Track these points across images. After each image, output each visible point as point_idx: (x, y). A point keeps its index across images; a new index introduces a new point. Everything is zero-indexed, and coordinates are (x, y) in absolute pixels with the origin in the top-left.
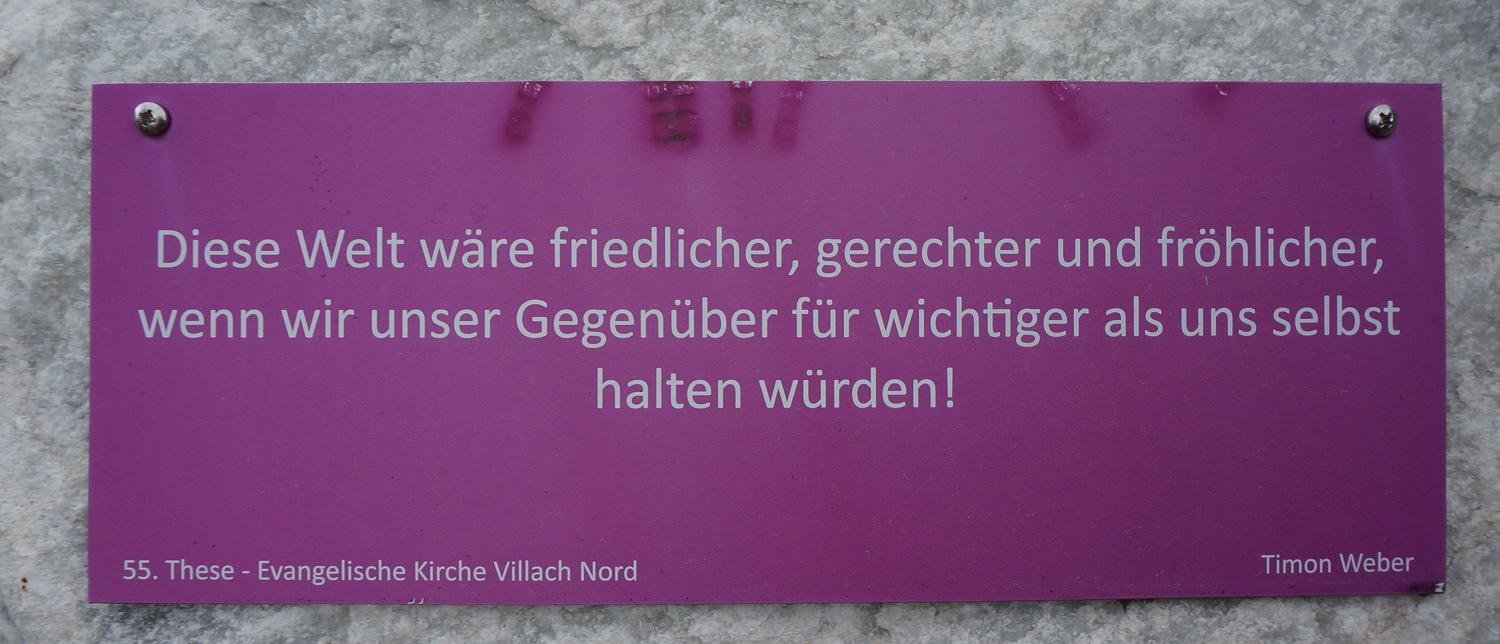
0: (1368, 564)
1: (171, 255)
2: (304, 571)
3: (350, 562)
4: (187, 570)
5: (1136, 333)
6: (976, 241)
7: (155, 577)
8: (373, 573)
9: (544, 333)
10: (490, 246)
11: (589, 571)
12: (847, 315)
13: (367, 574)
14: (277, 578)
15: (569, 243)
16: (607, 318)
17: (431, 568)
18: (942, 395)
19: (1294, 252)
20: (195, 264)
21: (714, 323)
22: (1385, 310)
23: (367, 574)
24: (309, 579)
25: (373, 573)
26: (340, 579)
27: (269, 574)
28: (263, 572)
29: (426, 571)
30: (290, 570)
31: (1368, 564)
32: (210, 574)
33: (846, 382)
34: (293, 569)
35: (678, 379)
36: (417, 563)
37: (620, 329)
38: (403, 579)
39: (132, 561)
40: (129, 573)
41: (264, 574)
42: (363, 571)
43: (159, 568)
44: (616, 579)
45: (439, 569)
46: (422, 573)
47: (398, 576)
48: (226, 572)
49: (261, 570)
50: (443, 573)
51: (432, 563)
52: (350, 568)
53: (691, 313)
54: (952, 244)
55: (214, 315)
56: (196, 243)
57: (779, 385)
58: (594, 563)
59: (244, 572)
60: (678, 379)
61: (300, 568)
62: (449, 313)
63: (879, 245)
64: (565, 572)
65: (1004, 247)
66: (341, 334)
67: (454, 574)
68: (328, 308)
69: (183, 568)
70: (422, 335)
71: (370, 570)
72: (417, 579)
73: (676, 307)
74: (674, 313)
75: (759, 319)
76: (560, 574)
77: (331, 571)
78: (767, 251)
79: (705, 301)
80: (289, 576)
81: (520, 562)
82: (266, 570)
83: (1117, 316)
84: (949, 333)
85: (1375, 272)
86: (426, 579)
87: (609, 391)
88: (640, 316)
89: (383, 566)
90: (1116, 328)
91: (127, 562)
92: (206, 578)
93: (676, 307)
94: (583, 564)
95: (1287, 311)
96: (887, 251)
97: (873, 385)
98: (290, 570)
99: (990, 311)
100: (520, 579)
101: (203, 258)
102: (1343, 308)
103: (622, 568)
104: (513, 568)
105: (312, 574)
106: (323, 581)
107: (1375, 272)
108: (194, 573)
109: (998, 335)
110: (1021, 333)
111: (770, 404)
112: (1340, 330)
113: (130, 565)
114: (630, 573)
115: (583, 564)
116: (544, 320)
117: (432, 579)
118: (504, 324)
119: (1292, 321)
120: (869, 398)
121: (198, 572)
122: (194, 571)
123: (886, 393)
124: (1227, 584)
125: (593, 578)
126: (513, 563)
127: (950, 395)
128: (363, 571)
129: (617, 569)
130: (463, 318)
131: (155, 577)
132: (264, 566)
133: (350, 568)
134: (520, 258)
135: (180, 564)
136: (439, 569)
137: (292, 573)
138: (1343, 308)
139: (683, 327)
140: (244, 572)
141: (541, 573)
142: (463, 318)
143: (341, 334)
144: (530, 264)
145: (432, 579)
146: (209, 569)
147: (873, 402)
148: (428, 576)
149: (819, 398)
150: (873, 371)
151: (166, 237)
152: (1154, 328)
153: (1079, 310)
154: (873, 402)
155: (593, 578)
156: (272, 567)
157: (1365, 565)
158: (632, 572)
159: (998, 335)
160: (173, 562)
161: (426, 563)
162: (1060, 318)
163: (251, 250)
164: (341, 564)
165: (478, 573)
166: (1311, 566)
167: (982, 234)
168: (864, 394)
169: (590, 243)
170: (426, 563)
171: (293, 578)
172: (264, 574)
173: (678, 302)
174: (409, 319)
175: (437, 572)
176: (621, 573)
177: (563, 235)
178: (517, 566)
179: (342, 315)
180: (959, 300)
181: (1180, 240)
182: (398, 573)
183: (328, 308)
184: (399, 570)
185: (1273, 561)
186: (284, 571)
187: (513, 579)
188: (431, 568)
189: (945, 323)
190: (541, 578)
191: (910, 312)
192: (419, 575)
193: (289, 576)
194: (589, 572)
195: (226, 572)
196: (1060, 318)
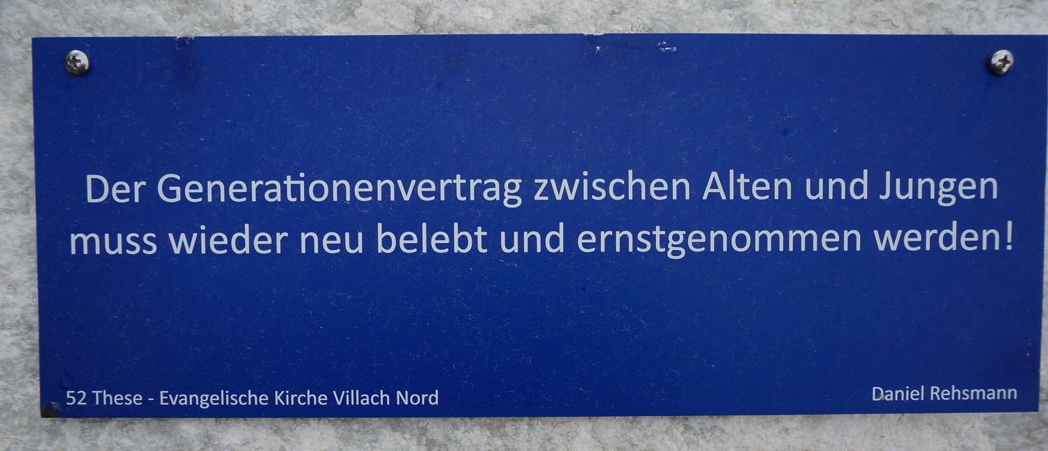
3: (227, 392)
4: (108, 398)
9: (178, 198)
14: (174, 403)
16: (956, 184)
17: (287, 396)
18: (1003, 241)
22: (654, 233)
25: (244, 400)
27: (168, 400)
28: (164, 399)
29: (283, 398)
30: (183, 397)
32: (125, 401)
33: (935, 231)
36: (276, 392)
37: (966, 192)
40: (71, 400)
44: (423, 403)
45: (293, 397)
48: (137, 399)
49: (162, 398)
50: (296, 399)
57: (888, 234)
59: (149, 399)
61: (999, 391)
62: (606, 181)
64: (385, 398)
67: (303, 400)
68: (585, 177)
69: (105, 397)
71: (243, 397)
72: (277, 404)
75: (274, 239)
80: (183, 402)
81: (352, 391)
82: (166, 398)
84: (623, 197)
86: (283, 404)
88: (332, 184)
89: (955, 389)
91: (68, 392)
92: (122, 403)
94: (399, 393)
95: (603, 181)
97: (246, 236)
98: (183, 397)
99: (289, 182)
100: (353, 403)
103: (296, 395)
104: (347, 396)
109: (295, 200)
110: (942, 196)
111: (881, 248)
113: (71, 394)
116: (178, 189)
117: (288, 404)
118: (148, 192)
120: (244, 247)
121: (116, 399)
123: (256, 242)
124: (854, 402)
125: (406, 403)
126: (347, 392)
127: (1009, 240)
129: (423, 396)
132: (164, 395)
133: (227, 396)
135: (103, 393)
136: (293, 397)
137: (185, 400)
140: (149, 399)
141: (368, 399)
145: (288, 404)
147: (953, 246)
148: (285, 402)
150: (955, 223)
153: (139, 182)
154: (953, 246)
155: (406, 403)
156: (170, 396)
158: (434, 398)
159: (295, 200)
161: (283, 392)
162: (124, 188)
163: (132, 398)
164: (248, 392)
165: (262, 399)
166: (319, 190)
168: (948, 239)
170: (283, 392)
171: (993, 398)
174: (986, 185)
176: (427, 399)
178: (350, 394)
180: (630, 172)
183: (585, 177)
184: (323, 397)
185: (101, 396)
186: (179, 398)
187: (348, 403)
188: (287, 396)
189: (620, 189)
191: (577, 181)
192: (279, 401)
193: (183, 402)
196: (124, 188)
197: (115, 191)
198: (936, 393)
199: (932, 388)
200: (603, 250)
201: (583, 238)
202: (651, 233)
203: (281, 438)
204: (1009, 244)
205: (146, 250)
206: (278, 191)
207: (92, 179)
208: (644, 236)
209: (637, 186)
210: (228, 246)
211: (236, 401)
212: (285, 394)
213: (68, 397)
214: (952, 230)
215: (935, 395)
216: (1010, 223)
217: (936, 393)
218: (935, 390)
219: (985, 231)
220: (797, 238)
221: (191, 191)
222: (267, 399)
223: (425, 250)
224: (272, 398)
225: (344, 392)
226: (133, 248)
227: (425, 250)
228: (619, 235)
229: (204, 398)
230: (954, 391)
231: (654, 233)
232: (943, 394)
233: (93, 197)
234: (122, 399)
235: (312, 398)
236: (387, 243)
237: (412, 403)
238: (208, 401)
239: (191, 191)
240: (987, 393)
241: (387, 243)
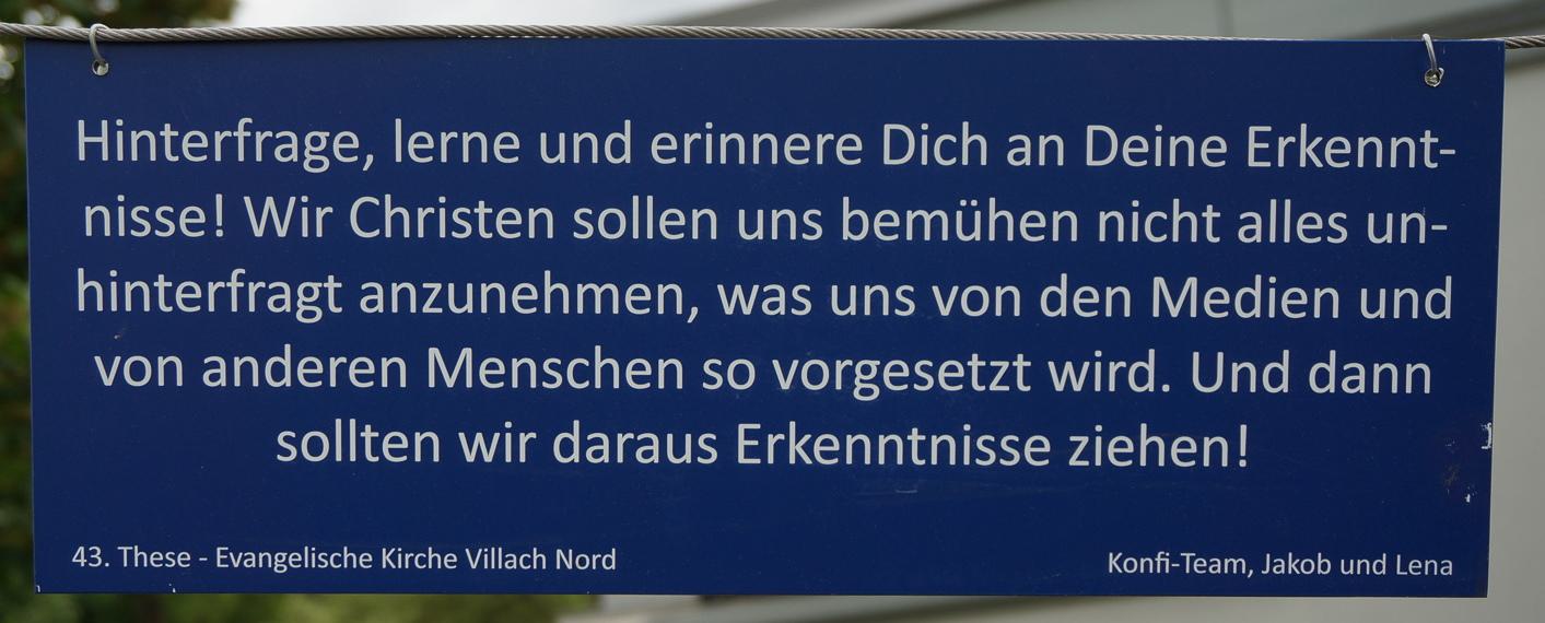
1: (1101, 152)
2: (265, 558)
3: (313, 549)
4: (141, 558)
5: (122, 233)
6: (1422, 140)
7: (107, 565)
8: (338, 560)
10: (1390, 144)
14: (236, 565)
15: (253, 136)
17: (400, 555)
19: (950, 150)
20: (924, 162)
22: (476, 210)
24: (270, 566)
27: (227, 561)
28: (221, 559)
29: (394, 558)
34: (515, 557)
35: (166, 280)
41: (223, 561)
43: (111, 555)
44: (594, 568)
45: (407, 556)
48: (182, 559)
49: (219, 557)
50: (412, 560)
51: (400, 550)
52: (313, 555)
53: (978, 214)
54: (966, 141)
55: (1057, 217)
56: (925, 138)
58: (571, 551)
60: (166, 280)
63: (821, 140)
65: (846, 143)
66: (319, 234)
67: (423, 561)
68: (442, 205)
69: (137, 555)
70: (793, 236)
72: (1111, 571)
73: (961, 208)
74: (959, 214)
77: (293, 559)
78: (1348, 150)
79: (992, 201)
81: (493, 549)
83: (1251, 221)
85: (365, 169)
86: (394, 567)
90: (1250, 233)
93: (961, 208)
96: (830, 147)
97: (1063, 292)
101: (493, 150)
102: (392, 208)
104: (486, 556)
105: (273, 560)
106: (285, 569)
107: (365, 169)
112: (1320, 571)
114: (609, 562)
115: (559, 552)
117: (400, 566)
119: (176, 220)
125: (570, 567)
126: (486, 550)
127: (1243, 453)
129: (595, 558)
130: (189, 215)
132: (223, 553)
134: (847, 155)
137: (252, 561)
138: (392, 208)
139: (968, 229)
141: (515, 561)
142: (189, 215)
143: (319, 234)
144: (1223, 163)
145: (400, 566)
146: (164, 555)
148: (396, 564)
151: (893, 132)
152: (812, 231)
155: (570, 567)
156: (231, 554)
158: (610, 560)
160: (125, 549)
161: (393, 550)
165: (363, 560)
167: (167, 126)
169: (704, 137)
170: (393, 550)
173: (963, 203)
175: (405, 560)
177: (247, 126)
179: (320, 213)
181: (258, 133)
182: (363, 560)
183: (442, 205)
186: (244, 558)
187: (486, 567)
188: (400, 555)
190: (515, 566)
195: (182, 559)
197: (1126, 150)
200: (211, 308)
201: (1305, 223)
202: (472, 211)
204: (1243, 458)
205: (160, 230)
207: (1095, 132)
208: (461, 216)
210: (1230, 307)
212: (396, 553)
214: (284, 358)
216: (219, 198)
219: (1064, 314)
220: (589, 295)
225: (480, 550)
226: (141, 228)
228: (467, 138)
229: (280, 558)
231: (476, 210)
233: (1095, 158)
234: (161, 558)
235: (435, 559)
236: (856, 225)
237: (586, 557)
238: (286, 563)
239: (1128, 150)
241: (856, 225)
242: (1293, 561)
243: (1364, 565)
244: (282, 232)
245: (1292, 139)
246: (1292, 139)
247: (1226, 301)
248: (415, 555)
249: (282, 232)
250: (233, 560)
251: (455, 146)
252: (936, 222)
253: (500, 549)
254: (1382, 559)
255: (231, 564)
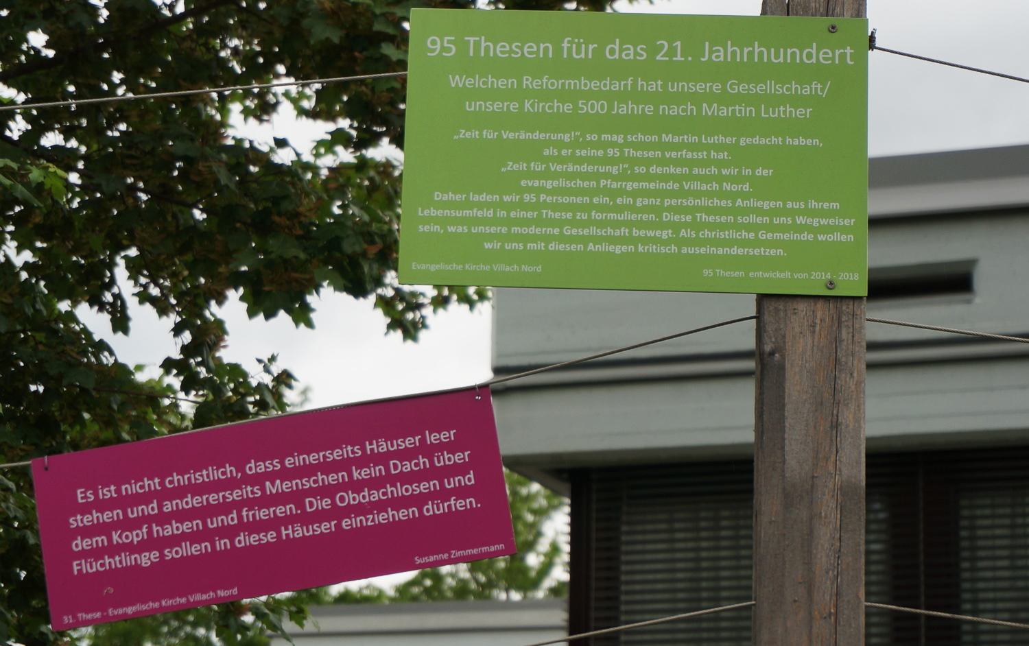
0: (469, 82)
4: (487, 48)
7: (479, 505)
11: (813, 204)
12: (591, 47)
13: (785, 90)
17: (536, 104)
21: (585, 85)
23: (785, 90)
26: (542, 87)
27: (86, 497)
31: (469, 82)
38: (517, 110)
39: (584, 102)
40: (582, 109)
41: (82, 498)
42: (782, 88)
45: (541, 105)
46: (530, 108)
47: (567, 110)
50: (544, 107)
64: (692, 109)
69: (483, 45)
72: (526, 110)
76: (689, 110)
86: (532, 111)
87: (642, 85)
96: (711, 87)
108: (796, 114)
112: (583, 88)
114: (539, 269)
116: (736, 87)
117: (536, 111)
121: (401, 515)
122: (587, 109)
128: (782, 88)
131: (299, 512)
141: (676, 110)
145: (536, 111)
148: (533, 108)
149: (791, 53)
157: (467, 83)
172: (82, 498)
188: (536, 104)
192: (528, 108)
194: (707, 109)
198: (528, 82)
199: (525, 77)
203: (47, 605)
206: (654, 86)
209: (493, 82)
210: (600, 87)
211: (488, 105)
212: (534, 102)
213: (580, 105)
215: (526, 84)
217: (528, 82)
218: (527, 80)
221: (743, 88)
222: (517, 106)
223: (477, 86)
224: (522, 106)
227: (477, 86)
228: (567, 82)
230: (390, 514)
232: (534, 84)
235: (558, 107)
240: (669, 109)
242: (356, 471)
243: (793, 54)
244: (461, 86)
245: (751, 49)
246: (751, 49)
247: (598, 85)
248: (713, 84)
249: (461, 86)
250: (685, 185)
251: (563, 84)
252: (575, 84)
253: (773, 82)
254: (607, 80)
255: (718, 107)
